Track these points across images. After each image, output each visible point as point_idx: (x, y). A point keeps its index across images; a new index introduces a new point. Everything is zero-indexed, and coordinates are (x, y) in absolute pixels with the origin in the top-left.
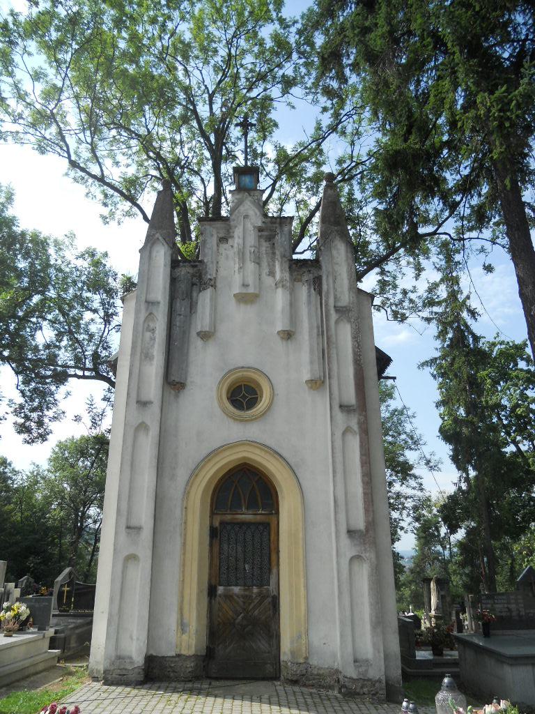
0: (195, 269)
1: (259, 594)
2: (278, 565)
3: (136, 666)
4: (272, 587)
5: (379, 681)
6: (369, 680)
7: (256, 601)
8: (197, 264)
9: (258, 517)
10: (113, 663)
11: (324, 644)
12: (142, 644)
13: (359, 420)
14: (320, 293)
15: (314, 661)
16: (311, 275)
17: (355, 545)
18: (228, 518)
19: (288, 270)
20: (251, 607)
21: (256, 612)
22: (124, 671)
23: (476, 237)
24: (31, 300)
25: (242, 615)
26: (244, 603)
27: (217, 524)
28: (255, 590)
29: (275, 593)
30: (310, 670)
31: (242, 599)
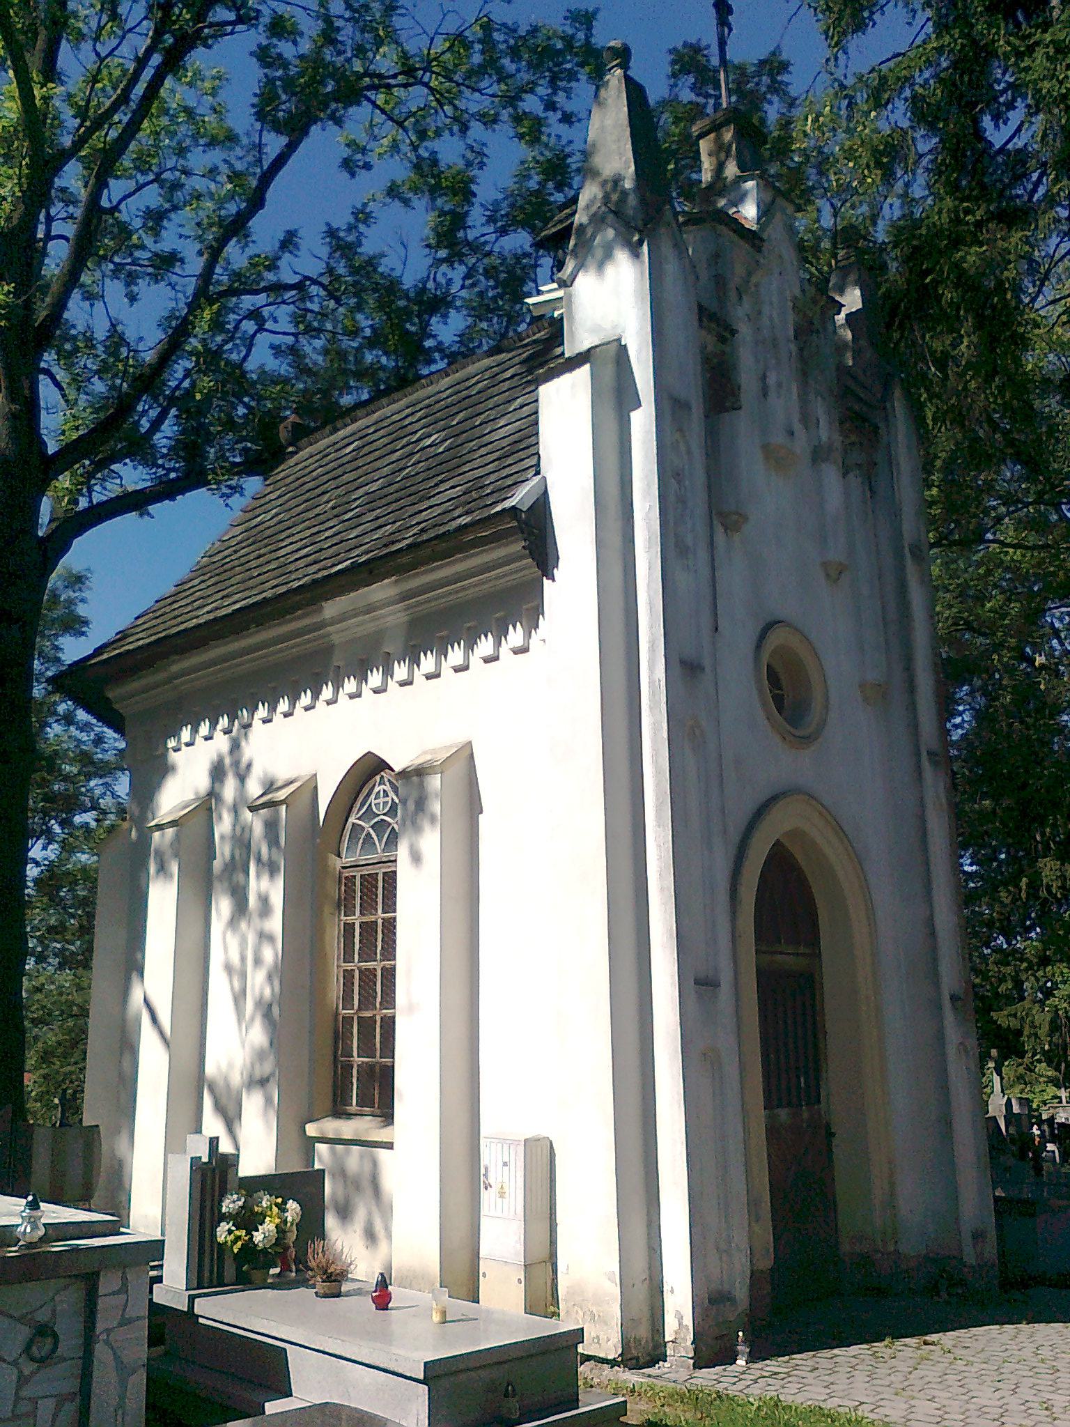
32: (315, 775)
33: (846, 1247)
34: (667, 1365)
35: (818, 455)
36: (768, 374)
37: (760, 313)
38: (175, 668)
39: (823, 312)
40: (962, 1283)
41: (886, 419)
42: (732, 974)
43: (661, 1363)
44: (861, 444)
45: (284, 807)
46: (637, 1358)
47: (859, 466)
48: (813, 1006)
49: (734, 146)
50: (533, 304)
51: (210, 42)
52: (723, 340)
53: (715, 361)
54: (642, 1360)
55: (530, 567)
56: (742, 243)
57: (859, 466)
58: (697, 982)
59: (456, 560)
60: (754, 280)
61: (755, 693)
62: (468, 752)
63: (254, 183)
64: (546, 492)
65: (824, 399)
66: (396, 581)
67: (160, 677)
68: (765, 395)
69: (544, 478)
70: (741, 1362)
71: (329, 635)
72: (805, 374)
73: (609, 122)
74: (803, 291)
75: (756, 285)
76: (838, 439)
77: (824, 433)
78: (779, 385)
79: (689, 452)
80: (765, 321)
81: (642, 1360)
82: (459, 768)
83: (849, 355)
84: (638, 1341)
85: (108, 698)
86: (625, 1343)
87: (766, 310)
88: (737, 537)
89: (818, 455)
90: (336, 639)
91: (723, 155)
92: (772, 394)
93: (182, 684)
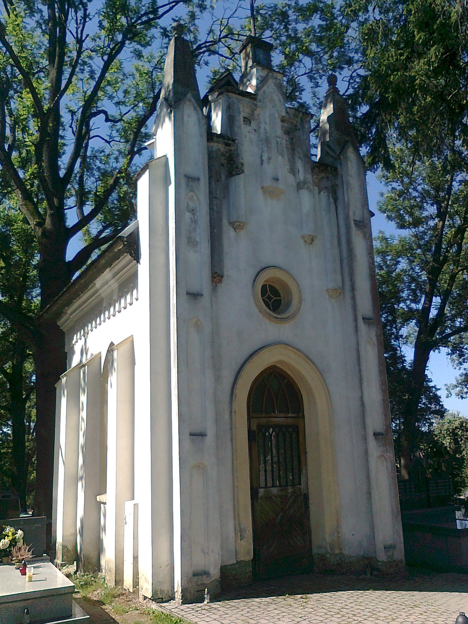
0: (227, 148)
1: (294, 492)
2: (306, 465)
3: (213, 579)
4: (303, 486)
5: (401, 561)
6: (394, 561)
7: (291, 500)
8: (230, 142)
9: (289, 420)
10: (190, 581)
11: (353, 535)
12: (217, 556)
13: (377, 332)
14: (336, 200)
15: (346, 552)
16: (329, 182)
17: (379, 446)
18: (264, 421)
19: (310, 171)
20: (287, 506)
21: (292, 511)
22: (304, 597)
23: (119, 140)
24: (61, 139)
25: (281, 514)
26: (282, 503)
27: (254, 428)
28: (290, 490)
29: (306, 491)
30: (343, 559)
31: (280, 500)
32: (100, 352)
33: (315, 551)
34: (174, 602)
35: (300, 186)
36: (263, 155)
37: (260, 127)
38: (69, 312)
39: (302, 120)
40: (378, 569)
41: (341, 164)
42: (366, 420)
43: (172, 601)
44: (327, 177)
45: (86, 367)
46: (162, 598)
47: (326, 188)
48: (298, 441)
49: (251, 53)
50: (148, 145)
51: (150, 43)
52: (227, 145)
53: (228, 154)
54: (164, 600)
55: (131, 262)
56: (244, 98)
57: (326, 188)
58: (191, 434)
59: (122, 259)
60: (256, 113)
61: (252, 301)
62: (132, 339)
63: (151, 101)
64: (138, 228)
65: (302, 160)
66: (110, 270)
67: (67, 316)
68: (262, 164)
69: (138, 221)
70: (205, 602)
71: (100, 294)
72: (293, 150)
73: (169, 60)
74: (287, 112)
75: (258, 115)
76: (309, 177)
77: (301, 176)
78: (270, 159)
79: (198, 200)
80: (262, 130)
81: (164, 600)
82: (127, 346)
83: (328, 136)
84: (162, 591)
85: (58, 326)
86: (154, 592)
87: (262, 126)
88: (242, 232)
89: (300, 186)
90: (103, 295)
91: (247, 58)
92: (265, 164)
93: (74, 317)
